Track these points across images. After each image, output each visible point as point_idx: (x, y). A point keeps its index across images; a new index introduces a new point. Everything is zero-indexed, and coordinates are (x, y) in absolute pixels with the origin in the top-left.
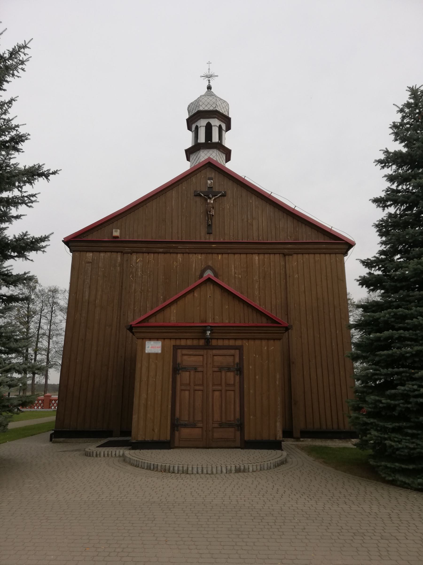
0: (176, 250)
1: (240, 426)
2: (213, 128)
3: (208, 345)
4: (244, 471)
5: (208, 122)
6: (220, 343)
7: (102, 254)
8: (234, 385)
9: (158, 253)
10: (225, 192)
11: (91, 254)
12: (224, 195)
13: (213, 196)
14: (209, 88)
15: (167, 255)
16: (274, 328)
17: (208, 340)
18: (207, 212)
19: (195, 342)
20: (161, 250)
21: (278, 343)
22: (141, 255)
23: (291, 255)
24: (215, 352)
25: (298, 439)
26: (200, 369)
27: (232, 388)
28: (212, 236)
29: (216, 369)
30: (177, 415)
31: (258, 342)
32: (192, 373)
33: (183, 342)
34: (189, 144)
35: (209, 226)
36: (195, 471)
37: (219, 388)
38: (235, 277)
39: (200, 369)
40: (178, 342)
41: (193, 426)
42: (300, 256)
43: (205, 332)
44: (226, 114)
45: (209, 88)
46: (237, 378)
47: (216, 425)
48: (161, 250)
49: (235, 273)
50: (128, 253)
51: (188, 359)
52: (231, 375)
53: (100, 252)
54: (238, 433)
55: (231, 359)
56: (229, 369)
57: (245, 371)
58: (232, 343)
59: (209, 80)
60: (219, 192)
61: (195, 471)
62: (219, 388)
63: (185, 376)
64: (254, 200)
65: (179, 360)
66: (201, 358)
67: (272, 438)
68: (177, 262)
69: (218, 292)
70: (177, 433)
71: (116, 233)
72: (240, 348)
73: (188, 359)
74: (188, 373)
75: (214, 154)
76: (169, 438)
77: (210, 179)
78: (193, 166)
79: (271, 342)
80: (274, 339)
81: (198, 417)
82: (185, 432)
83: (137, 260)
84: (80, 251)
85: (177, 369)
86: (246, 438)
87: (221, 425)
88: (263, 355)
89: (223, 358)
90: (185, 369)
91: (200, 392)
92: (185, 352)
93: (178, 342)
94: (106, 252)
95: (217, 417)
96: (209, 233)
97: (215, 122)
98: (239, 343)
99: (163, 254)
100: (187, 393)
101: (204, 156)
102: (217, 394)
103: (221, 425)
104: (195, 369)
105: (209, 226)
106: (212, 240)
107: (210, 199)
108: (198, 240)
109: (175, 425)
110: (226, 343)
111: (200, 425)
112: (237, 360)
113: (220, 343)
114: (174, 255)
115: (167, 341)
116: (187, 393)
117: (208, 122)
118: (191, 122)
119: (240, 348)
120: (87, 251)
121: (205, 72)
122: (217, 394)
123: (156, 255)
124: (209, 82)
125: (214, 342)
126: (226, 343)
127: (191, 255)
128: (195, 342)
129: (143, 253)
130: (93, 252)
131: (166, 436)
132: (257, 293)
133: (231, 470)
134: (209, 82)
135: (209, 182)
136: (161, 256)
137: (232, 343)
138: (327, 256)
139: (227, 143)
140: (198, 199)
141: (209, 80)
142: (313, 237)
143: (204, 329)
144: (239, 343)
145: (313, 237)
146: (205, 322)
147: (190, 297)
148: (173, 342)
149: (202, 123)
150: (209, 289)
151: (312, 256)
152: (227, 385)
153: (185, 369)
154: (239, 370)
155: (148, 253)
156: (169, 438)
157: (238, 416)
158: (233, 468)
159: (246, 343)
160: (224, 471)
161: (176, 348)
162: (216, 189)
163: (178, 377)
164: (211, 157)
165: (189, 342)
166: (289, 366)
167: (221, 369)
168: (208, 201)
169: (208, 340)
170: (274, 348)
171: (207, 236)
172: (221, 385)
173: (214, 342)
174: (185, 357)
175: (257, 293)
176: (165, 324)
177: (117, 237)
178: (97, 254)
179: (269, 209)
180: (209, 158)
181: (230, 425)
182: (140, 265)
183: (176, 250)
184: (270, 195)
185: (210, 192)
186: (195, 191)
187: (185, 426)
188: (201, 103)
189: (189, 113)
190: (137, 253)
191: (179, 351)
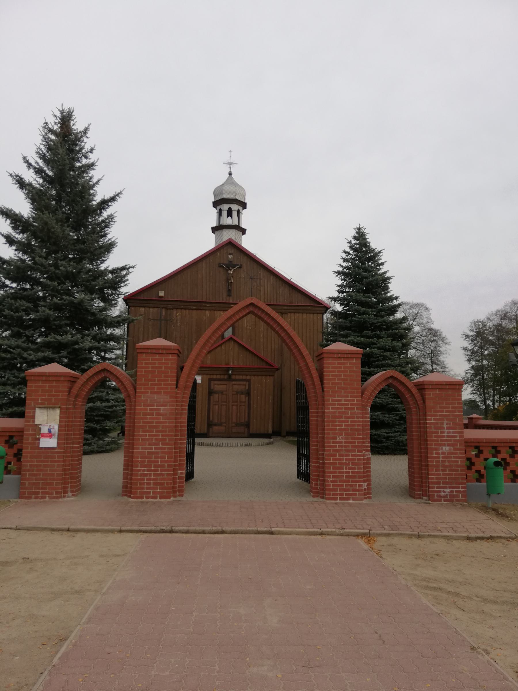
0: (205, 308)
1: (248, 425)
2: (233, 212)
3: (230, 378)
4: (249, 446)
5: (228, 204)
6: (237, 377)
7: (151, 309)
8: (245, 402)
9: (192, 309)
10: (241, 265)
11: (143, 309)
12: (240, 267)
13: (233, 268)
14: (230, 174)
15: (199, 311)
16: (269, 369)
17: (230, 376)
18: (228, 280)
19: (222, 377)
20: (194, 307)
21: (272, 378)
22: (179, 310)
23: (287, 314)
24: (234, 383)
25: (284, 437)
26: (224, 393)
27: (243, 404)
28: (231, 298)
29: (234, 393)
30: (211, 419)
31: (260, 377)
32: (220, 395)
33: (215, 377)
34: (215, 224)
35: (229, 291)
36: (224, 445)
37: (236, 404)
38: (247, 328)
39: (224, 393)
40: (211, 377)
41: (220, 425)
42: (292, 314)
43: (228, 371)
44: (243, 201)
45: (230, 174)
46: (247, 398)
47: (233, 425)
48: (194, 307)
49: (247, 326)
50: (170, 309)
51: (218, 387)
52: (243, 396)
53: (149, 307)
54: (246, 430)
55: (244, 387)
56: (242, 393)
57: (252, 394)
58: (244, 377)
59: (230, 167)
60: (237, 265)
61: (224, 445)
62: (236, 404)
63: (216, 396)
64: (262, 273)
65: (212, 387)
66: (225, 386)
67: (266, 432)
68: (205, 316)
69: (236, 346)
70: (211, 429)
71: (162, 294)
72: (249, 381)
73: (218, 387)
74: (217, 395)
75: (233, 234)
76: (206, 432)
77: (230, 254)
78: (217, 245)
79: (268, 377)
80: (270, 376)
81: (223, 420)
82: (216, 428)
83: (177, 314)
84: (135, 307)
85: (211, 393)
86: (251, 432)
87: (237, 425)
88: (263, 385)
89: (238, 387)
90: (216, 392)
91: (225, 406)
92: (216, 382)
93: (211, 377)
94: (154, 307)
95: (234, 420)
96: (229, 296)
97: (235, 207)
98: (248, 377)
99: (195, 311)
100: (217, 406)
101: (227, 235)
102: (235, 407)
103: (237, 425)
104: (222, 393)
105: (229, 291)
106: (231, 301)
107: (230, 270)
108: (221, 301)
109: (210, 425)
110: (241, 377)
111: (224, 425)
112: (247, 388)
113: (237, 377)
114: (203, 311)
115: (205, 376)
116: (217, 406)
117: (228, 204)
118: (215, 204)
119: (249, 381)
120: (140, 307)
121: (227, 160)
122: (235, 407)
123: (191, 311)
124: (230, 169)
125: (233, 377)
126: (241, 377)
127: (216, 312)
128: (222, 377)
129: (181, 309)
130: (144, 307)
131: (205, 431)
132: (261, 340)
133: (242, 445)
134: (230, 169)
135: (230, 257)
136: (194, 312)
137: (244, 377)
138: (312, 315)
139: (243, 225)
140: (221, 269)
141: (230, 167)
142: (303, 302)
143: (228, 369)
144: (248, 377)
145: (303, 302)
146: (228, 364)
147: (219, 348)
148: (208, 377)
149: (225, 207)
150: (232, 343)
151: (301, 315)
152: (241, 402)
153: (216, 392)
154: (248, 393)
155: (185, 309)
156: (206, 432)
157: (246, 419)
158: (244, 444)
159: (253, 378)
160: (239, 445)
161: (210, 380)
162: (235, 262)
163: (212, 397)
164: (233, 238)
165: (218, 377)
166: (281, 390)
167: (237, 393)
168: (229, 272)
169: (230, 376)
170: (269, 381)
171: (228, 298)
172: (237, 402)
173: (233, 377)
174: (216, 386)
175: (261, 340)
176: (204, 366)
177: (162, 297)
178: (147, 309)
179: (272, 279)
180: (230, 239)
181: (241, 425)
182: (179, 318)
183: (205, 308)
184: (273, 269)
185: (230, 265)
186: (219, 264)
187: (216, 425)
188: (224, 192)
189: (215, 196)
190: (177, 309)
191: (212, 382)
